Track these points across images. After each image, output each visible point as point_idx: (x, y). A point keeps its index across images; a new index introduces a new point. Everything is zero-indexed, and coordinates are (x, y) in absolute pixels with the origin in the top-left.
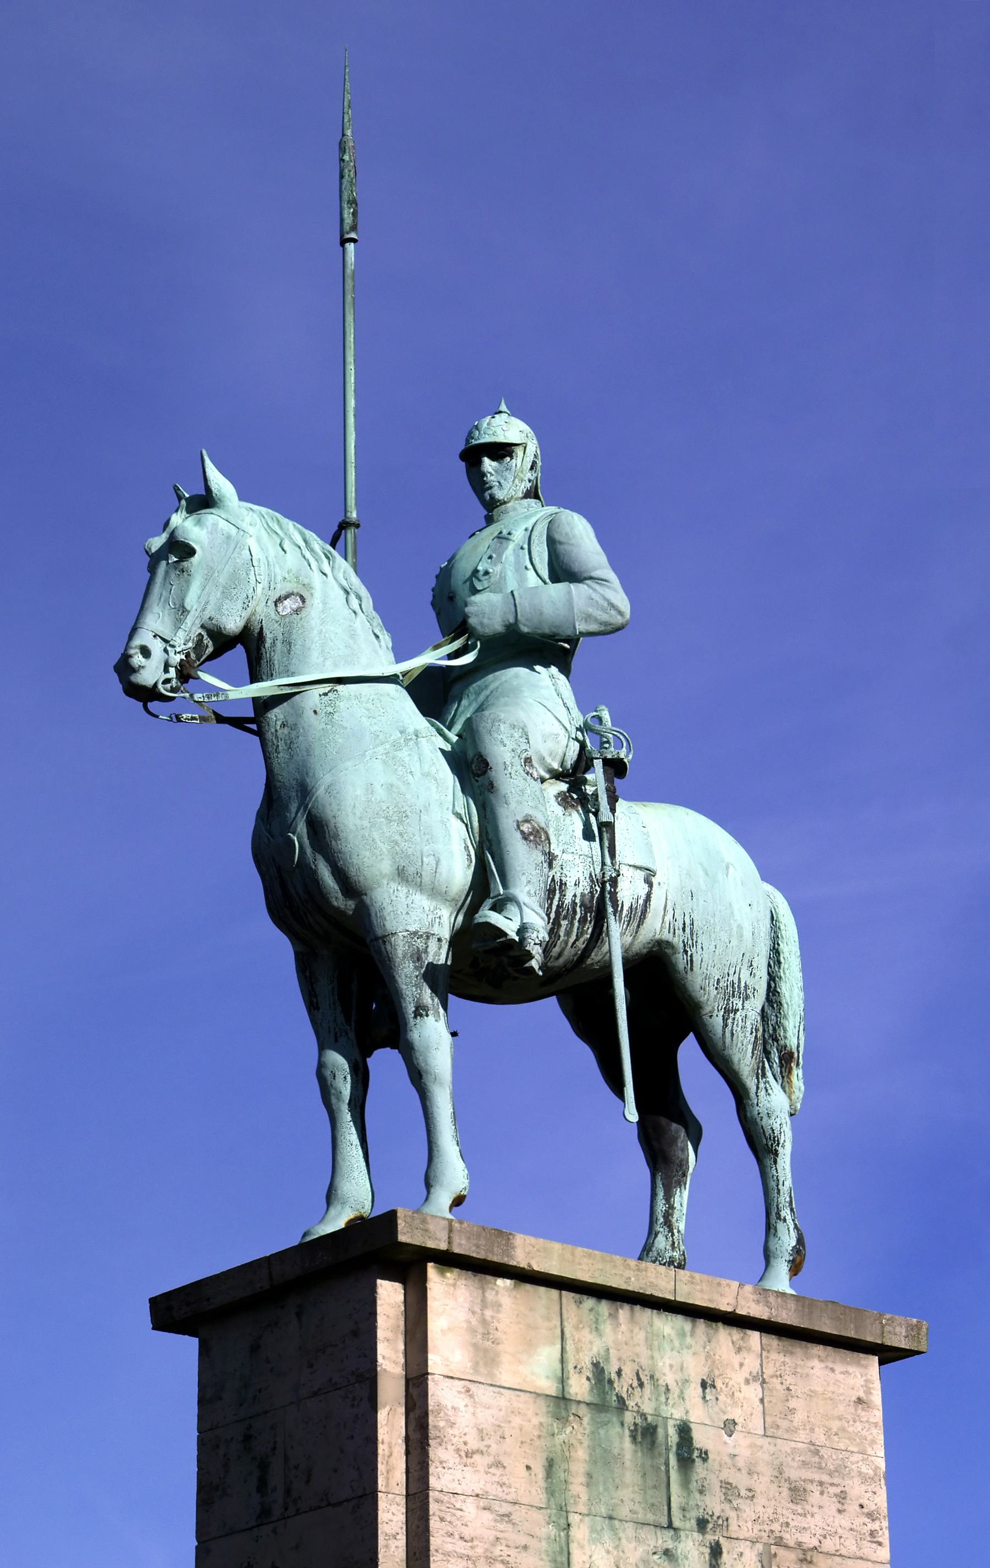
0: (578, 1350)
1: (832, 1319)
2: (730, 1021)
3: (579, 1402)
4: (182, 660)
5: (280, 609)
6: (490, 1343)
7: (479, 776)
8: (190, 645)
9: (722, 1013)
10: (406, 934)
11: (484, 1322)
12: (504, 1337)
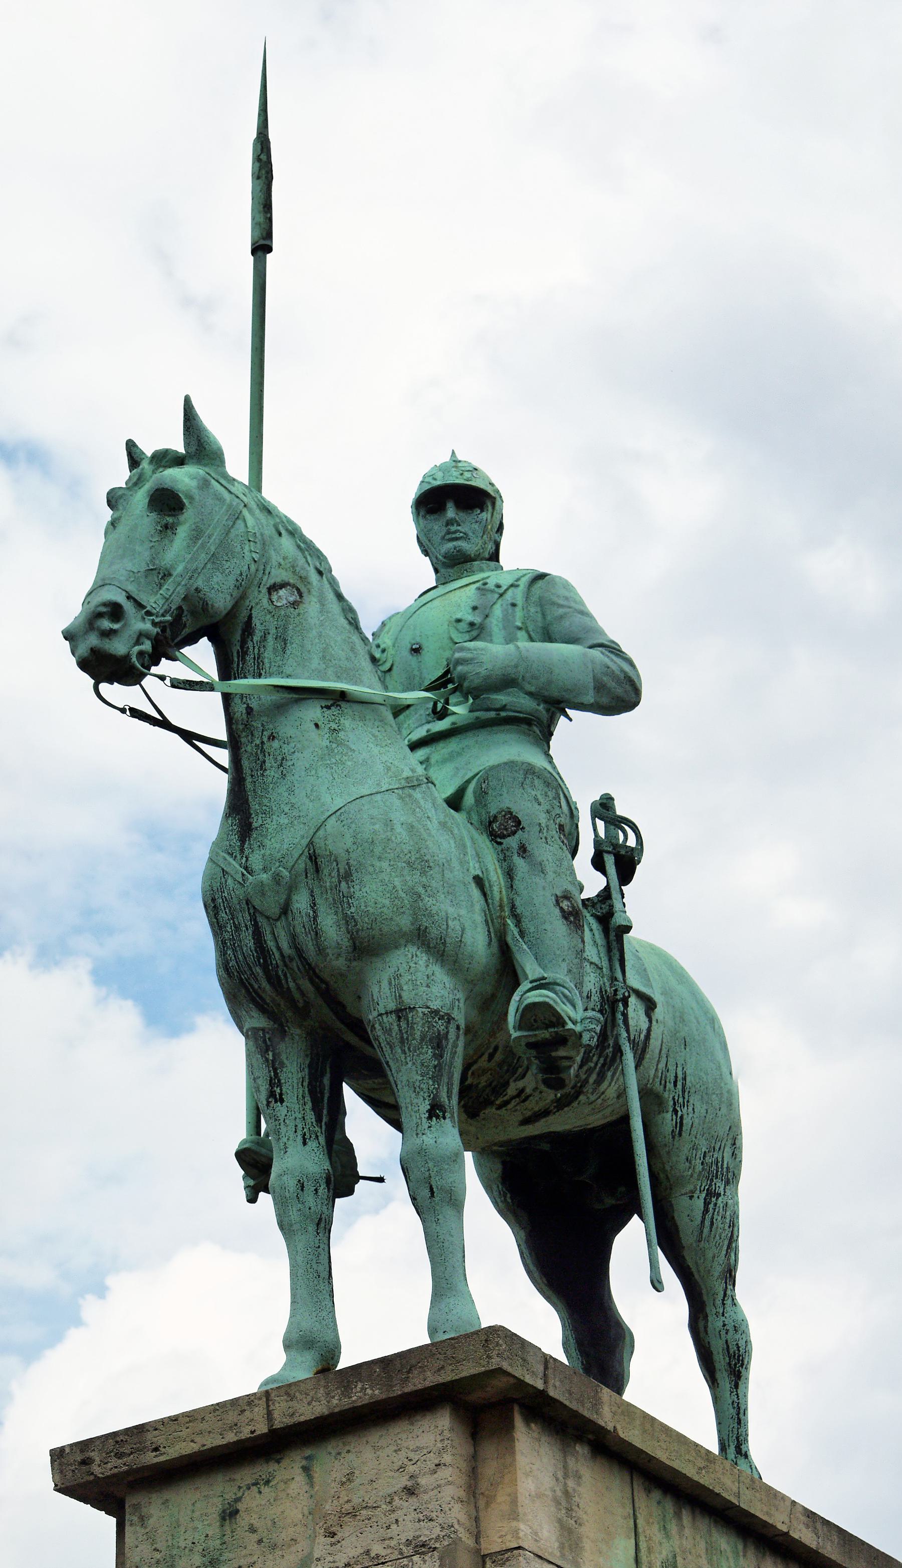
0: (650, 1550)
1: (868, 1562)
2: (711, 1206)
4: (158, 633)
5: (274, 597)
6: (573, 1522)
7: (504, 837)
9: (704, 1195)
10: (426, 1011)
11: (566, 1493)
12: (584, 1516)
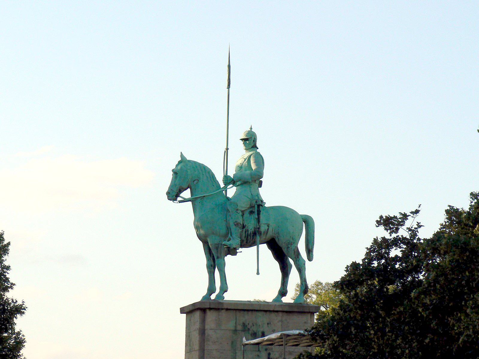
2: (288, 250)
3: (239, 330)
8: (178, 191)
